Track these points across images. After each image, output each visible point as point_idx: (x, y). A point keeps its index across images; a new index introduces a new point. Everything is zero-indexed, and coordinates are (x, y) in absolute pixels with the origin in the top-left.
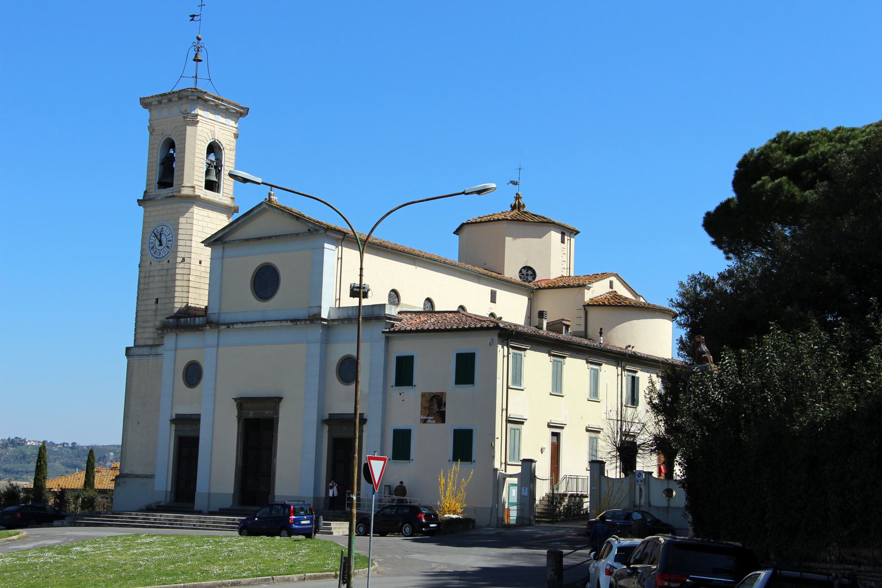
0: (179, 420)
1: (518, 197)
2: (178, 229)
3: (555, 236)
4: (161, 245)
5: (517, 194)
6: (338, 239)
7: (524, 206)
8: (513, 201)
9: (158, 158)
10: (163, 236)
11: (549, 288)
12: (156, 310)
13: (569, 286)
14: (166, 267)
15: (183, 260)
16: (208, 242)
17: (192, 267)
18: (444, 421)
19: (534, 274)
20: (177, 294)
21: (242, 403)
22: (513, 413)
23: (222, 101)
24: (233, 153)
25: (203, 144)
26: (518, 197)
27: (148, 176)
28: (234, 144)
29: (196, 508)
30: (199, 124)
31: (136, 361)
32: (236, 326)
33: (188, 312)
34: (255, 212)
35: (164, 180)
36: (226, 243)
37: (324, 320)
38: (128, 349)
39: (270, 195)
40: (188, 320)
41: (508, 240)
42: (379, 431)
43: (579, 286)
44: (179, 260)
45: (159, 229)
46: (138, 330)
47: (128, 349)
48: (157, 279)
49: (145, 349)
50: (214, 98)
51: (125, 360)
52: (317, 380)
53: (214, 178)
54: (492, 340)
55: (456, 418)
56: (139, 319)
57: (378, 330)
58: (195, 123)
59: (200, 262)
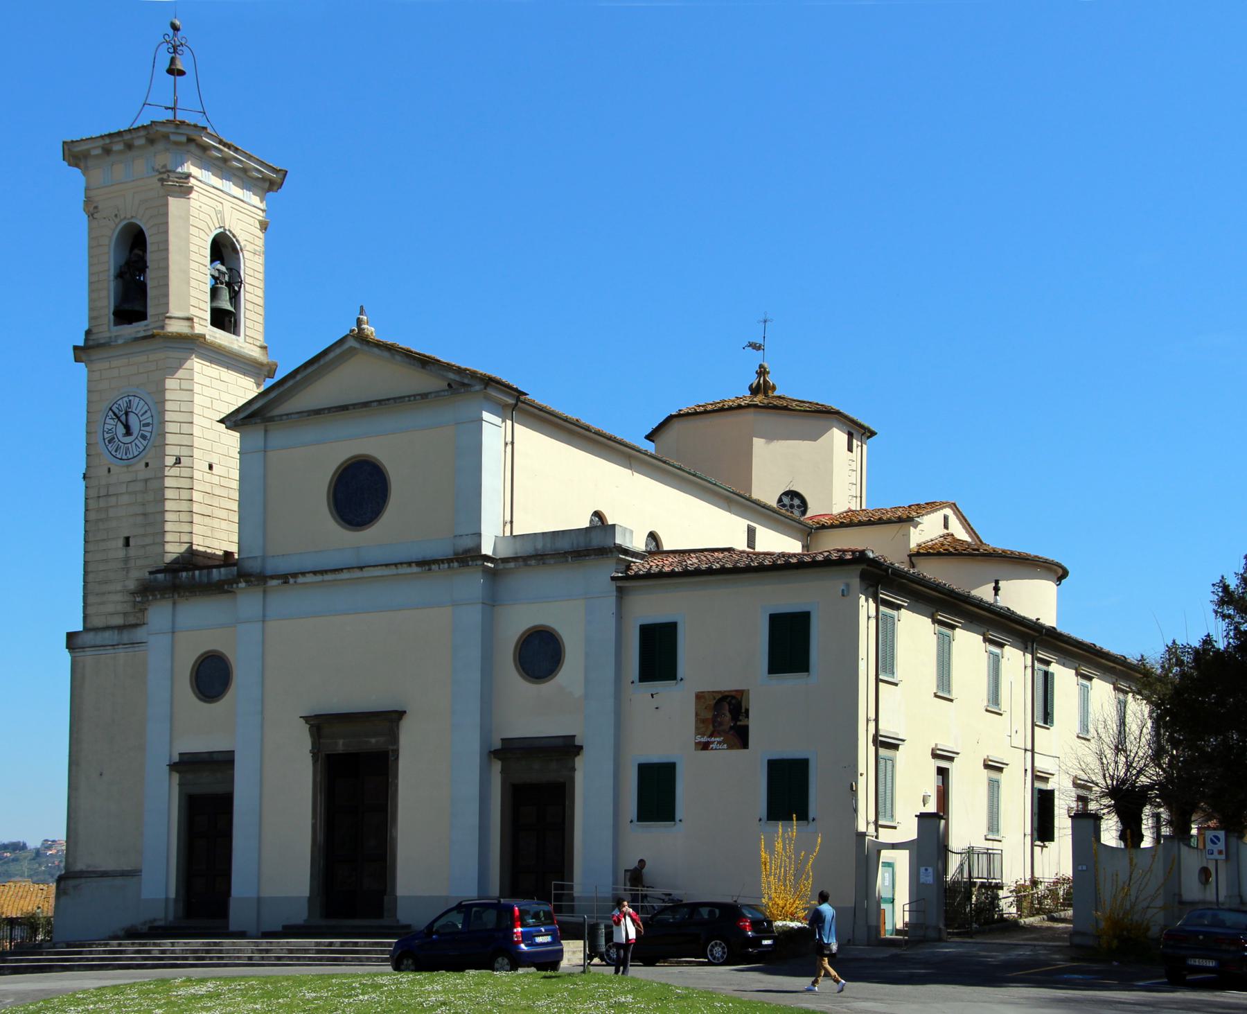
0: (186, 765)
1: (762, 372)
2: (164, 401)
3: (838, 437)
4: (128, 432)
5: (761, 366)
6: (505, 406)
7: (774, 388)
8: (754, 380)
9: (110, 263)
10: (132, 416)
11: (832, 526)
12: (126, 560)
13: (880, 522)
14: (141, 476)
15: (178, 461)
16: (233, 421)
17: (197, 475)
18: (745, 744)
19: (804, 505)
20: (168, 527)
21: (320, 725)
22: (888, 728)
23: (236, 150)
24: (261, 260)
25: (203, 235)
26: (762, 372)
27: (91, 300)
28: (260, 243)
29: (233, 927)
30: (193, 195)
31: (88, 657)
32: (301, 579)
33: (192, 560)
34: (331, 355)
35: (127, 307)
36: (271, 419)
37: (487, 558)
38: (71, 636)
39: (359, 322)
40: (194, 575)
41: (758, 443)
42: (609, 766)
43: (900, 520)
44: (170, 461)
45: (123, 403)
46: (91, 599)
47: (71, 636)
48: (125, 499)
49: (107, 634)
50: (221, 142)
51: (66, 657)
52: (477, 675)
53: (226, 305)
54: (848, 585)
55: (772, 736)
56: (91, 577)
57: (602, 574)
58: (185, 191)
59: (211, 467)
